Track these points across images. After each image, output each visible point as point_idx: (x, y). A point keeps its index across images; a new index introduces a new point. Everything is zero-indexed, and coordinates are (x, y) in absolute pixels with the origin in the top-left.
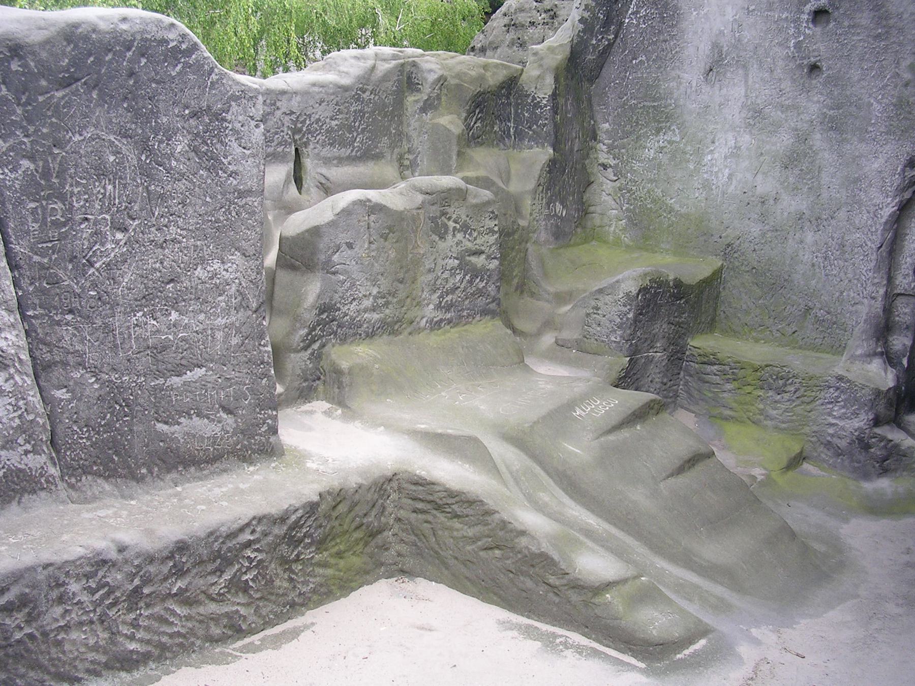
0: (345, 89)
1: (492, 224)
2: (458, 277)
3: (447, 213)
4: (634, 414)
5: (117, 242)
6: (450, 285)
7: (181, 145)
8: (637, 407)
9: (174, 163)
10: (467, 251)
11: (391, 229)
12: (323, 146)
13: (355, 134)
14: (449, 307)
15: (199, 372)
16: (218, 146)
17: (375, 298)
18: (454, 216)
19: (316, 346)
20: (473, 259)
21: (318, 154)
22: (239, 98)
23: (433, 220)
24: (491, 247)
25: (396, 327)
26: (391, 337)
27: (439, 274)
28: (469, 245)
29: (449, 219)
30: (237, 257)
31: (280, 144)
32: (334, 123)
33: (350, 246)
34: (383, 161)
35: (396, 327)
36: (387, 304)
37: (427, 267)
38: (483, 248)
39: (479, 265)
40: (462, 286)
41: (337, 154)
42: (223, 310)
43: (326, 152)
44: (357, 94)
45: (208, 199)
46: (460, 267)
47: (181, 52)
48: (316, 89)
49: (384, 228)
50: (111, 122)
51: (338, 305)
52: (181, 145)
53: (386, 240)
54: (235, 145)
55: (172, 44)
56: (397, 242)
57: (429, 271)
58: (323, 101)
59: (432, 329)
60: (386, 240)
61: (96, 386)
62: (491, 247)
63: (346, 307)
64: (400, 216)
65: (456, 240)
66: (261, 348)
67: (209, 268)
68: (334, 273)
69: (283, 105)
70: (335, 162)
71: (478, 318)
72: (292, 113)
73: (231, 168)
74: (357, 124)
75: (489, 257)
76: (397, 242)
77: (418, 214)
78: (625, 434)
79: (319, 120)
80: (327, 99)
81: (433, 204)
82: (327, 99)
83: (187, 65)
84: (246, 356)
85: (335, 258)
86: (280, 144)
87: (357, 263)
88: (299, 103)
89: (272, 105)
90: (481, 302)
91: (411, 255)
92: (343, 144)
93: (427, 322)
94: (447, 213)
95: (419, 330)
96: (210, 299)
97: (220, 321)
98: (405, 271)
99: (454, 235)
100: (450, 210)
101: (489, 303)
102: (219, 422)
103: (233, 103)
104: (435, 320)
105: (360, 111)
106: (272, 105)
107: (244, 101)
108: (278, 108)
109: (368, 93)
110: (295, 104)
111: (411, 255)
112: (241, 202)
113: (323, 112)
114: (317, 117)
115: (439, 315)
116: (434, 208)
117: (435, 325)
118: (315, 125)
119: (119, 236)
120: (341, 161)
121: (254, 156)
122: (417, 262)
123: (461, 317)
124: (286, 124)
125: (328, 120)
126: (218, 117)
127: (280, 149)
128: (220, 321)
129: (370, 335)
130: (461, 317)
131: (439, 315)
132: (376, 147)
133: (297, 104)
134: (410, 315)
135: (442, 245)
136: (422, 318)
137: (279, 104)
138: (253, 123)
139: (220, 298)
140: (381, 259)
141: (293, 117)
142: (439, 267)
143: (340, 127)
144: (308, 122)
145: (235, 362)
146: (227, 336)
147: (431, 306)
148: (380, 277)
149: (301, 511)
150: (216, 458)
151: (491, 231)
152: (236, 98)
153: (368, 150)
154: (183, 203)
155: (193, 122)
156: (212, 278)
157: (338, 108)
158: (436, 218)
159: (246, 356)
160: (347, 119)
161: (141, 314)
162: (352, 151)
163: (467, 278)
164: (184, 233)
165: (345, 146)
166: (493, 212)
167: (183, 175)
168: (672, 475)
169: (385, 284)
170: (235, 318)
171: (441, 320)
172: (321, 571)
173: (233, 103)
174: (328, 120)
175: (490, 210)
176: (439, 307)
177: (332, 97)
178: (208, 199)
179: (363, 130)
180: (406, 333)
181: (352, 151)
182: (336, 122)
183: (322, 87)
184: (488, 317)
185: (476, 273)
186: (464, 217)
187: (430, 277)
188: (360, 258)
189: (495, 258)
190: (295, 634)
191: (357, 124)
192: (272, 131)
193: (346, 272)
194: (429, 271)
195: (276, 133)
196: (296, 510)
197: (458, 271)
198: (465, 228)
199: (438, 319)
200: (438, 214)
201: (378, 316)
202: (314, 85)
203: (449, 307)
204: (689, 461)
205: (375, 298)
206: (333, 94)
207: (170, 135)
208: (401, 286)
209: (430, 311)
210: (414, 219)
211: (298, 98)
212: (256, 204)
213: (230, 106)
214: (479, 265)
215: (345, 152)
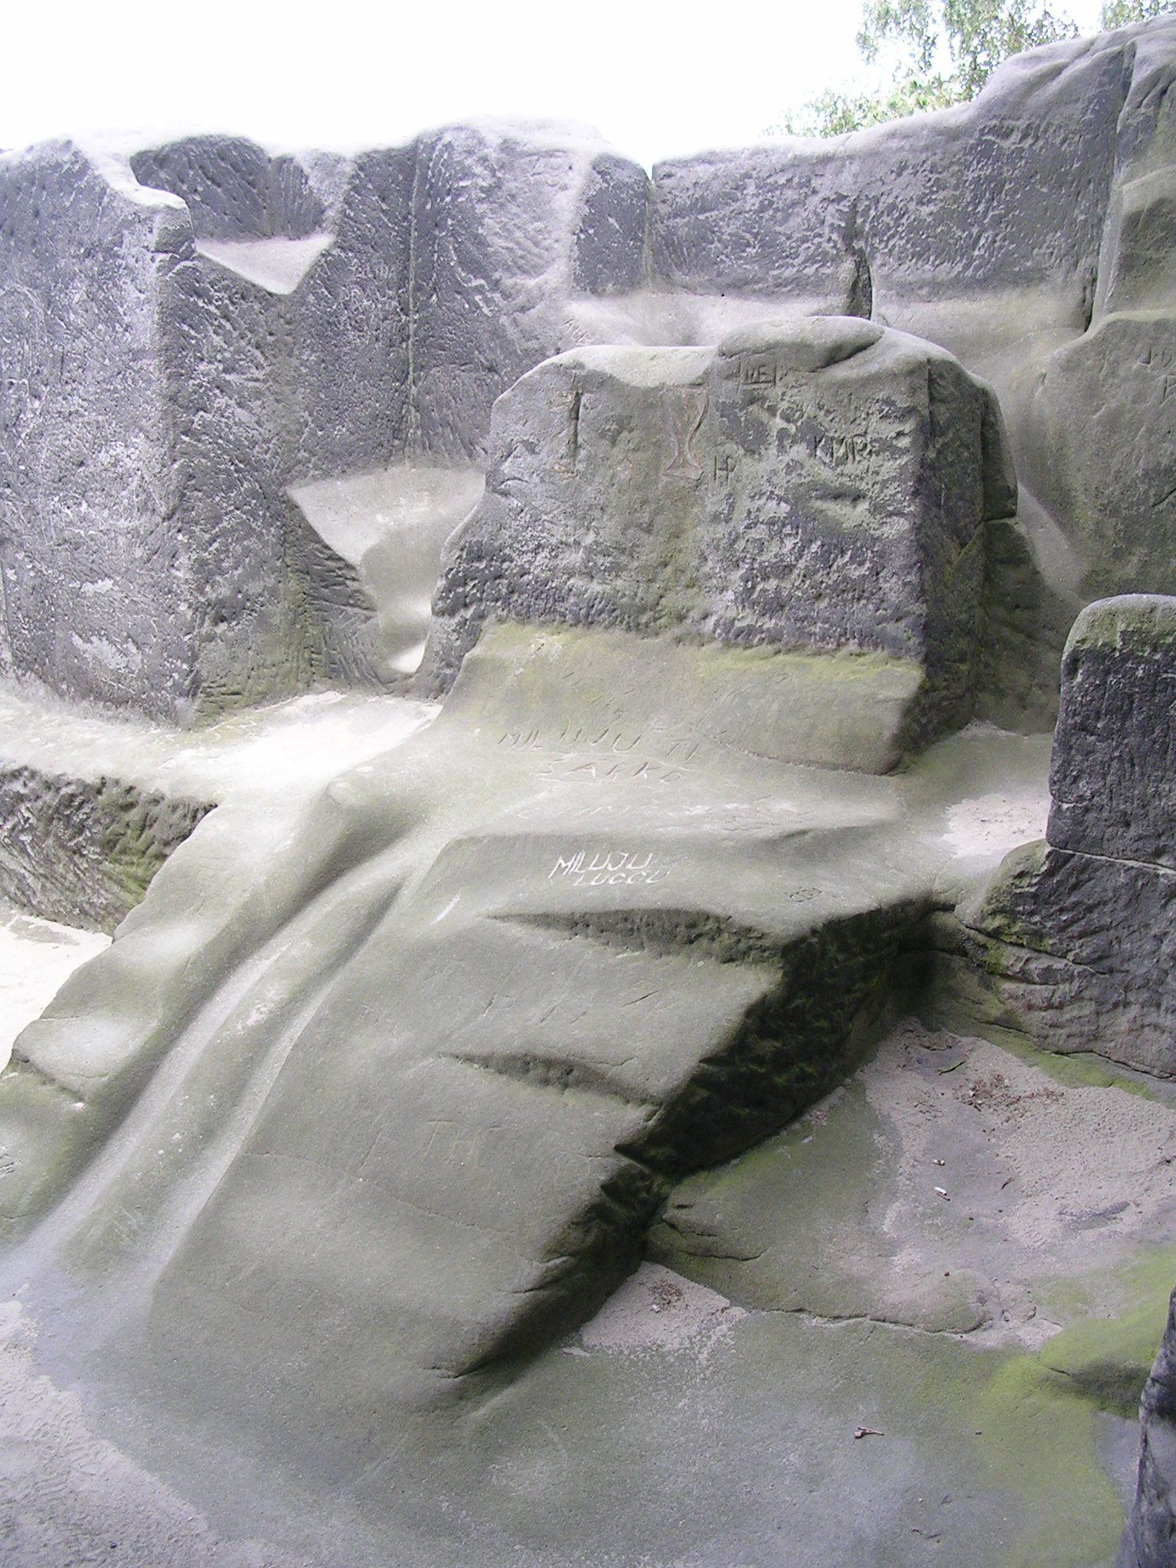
0: (952, 135)
1: (889, 430)
2: (789, 543)
3: (764, 399)
4: (626, 916)
5: (34, 411)
6: (768, 557)
7: (78, 294)
8: (643, 905)
9: (72, 317)
10: (814, 486)
11: (624, 424)
12: (901, 260)
13: (975, 231)
14: (775, 606)
15: (108, 584)
16: (114, 291)
17: (589, 550)
18: (784, 405)
19: (469, 613)
20: (835, 509)
21: (887, 277)
22: (132, 223)
23: (725, 410)
24: (884, 484)
25: (644, 619)
26: (632, 635)
27: (741, 529)
28: (826, 474)
29: (772, 411)
30: (140, 440)
31: (810, 260)
32: (925, 210)
33: (531, 448)
34: (1042, 287)
35: (644, 619)
36: (616, 569)
37: (710, 509)
38: (863, 486)
39: (847, 525)
40: (801, 564)
41: (928, 276)
42: (126, 509)
43: (906, 272)
44: (980, 142)
45: (107, 362)
46: (793, 520)
47: (74, 175)
48: (894, 144)
49: (607, 420)
50: (22, 272)
51: (507, 551)
52: (78, 294)
53: (613, 443)
54: (130, 287)
55: (66, 167)
56: (635, 450)
57: (715, 518)
58: (905, 168)
59: (728, 645)
60: (613, 443)
61: (32, 574)
62: (884, 484)
63: (526, 558)
64: (650, 400)
65: (786, 459)
66: (173, 571)
67: (112, 452)
68: (505, 494)
69: (825, 185)
70: (924, 292)
71: (853, 646)
72: (841, 198)
73: (127, 319)
74: (981, 208)
75: (876, 509)
76: (635, 450)
77: (691, 396)
78: (553, 942)
79: (893, 207)
80: (912, 162)
81: (728, 377)
82: (912, 162)
83: (80, 191)
84: (152, 577)
85: (506, 467)
86: (810, 260)
87: (542, 481)
88: (856, 176)
89: (801, 186)
90: (863, 612)
91: (665, 479)
92: (945, 254)
93: (716, 625)
94: (764, 399)
95: (701, 640)
96: (113, 492)
97: (123, 523)
98: (657, 512)
99: (781, 448)
100: (775, 392)
101: (884, 619)
102: (126, 655)
103: (126, 232)
104: (738, 624)
105: (989, 179)
106: (801, 186)
107: (138, 226)
108: (815, 192)
109: (1015, 137)
110: (847, 181)
111: (665, 479)
112: (136, 366)
113: (904, 189)
114: (890, 200)
115: (747, 618)
116: (730, 385)
117: (738, 637)
118: (885, 219)
119: (37, 404)
120: (936, 289)
121: (148, 301)
122: (687, 495)
123: (802, 634)
124: (829, 220)
125: (912, 206)
126: (110, 254)
127: (810, 271)
128: (123, 523)
129: (586, 619)
130: (802, 634)
131: (747, 618)
132: (1026, 257)
133: (850, 179)
134: (674, 600)
135: (748, 467)
136: (705, 617)
137: (816, 183)
138: (149, 255)
139: (124, 493)
140: (597, 479)
141: (844, 206)
142: (740, 515)
143: (940, 218)
144: (872, 213)
145: (140, 582)
146: (131, 545)
147: (730, 595)
148: (597, 513)
149: (73, 787)
150: (120, 702)
151: (887, 447)
152: (127, 224)
153: (1002, 265)
154: (82, 367)
155: (88, 262)
156: (114, 465)
157: (934, 177)
158: (734, 405)
159: (152, 577)
160: (956, 200)
161: (56, 499)
162: (966, 267)
163: (814, 547)
164: (85, 404)
165: (951, 260)
166: (888, 402)
167: (80, 331)
168: (486, 1062)
169: (609, 529)
170: (142, 522)
171: (750, 631)
172: (116, 888)
173: (126, 232)
174: (912, 206)
175: (881, 396)
176: (745, 598)
177: (924, 156)
178: (107, 362)
179: (998, 221)
180: (668, 635)
181: (966, 267)
182: (932, 208)
183: (906, 137)
184: (881, 654)
185: (837, 542)
186: (809, 410)
187: (721, 530)
188: (551, 473)
189: (899, 513)
190: (54, 938)
191: (981, 208)
192: (796, 236)
193: (521, 494)
194: (715, 518)
195: (805, 240)
196: (69, 784)
197: (788, 530)
198: (815, 438)
199: (744, 624)
200: (738, 398)
201: (599, 588)
202: (892, 135)
203: (775, 606)
204: (549, 1063)
205: (589, 550)
206: (926, 148)
207: (66, 280)
208: (648, 539)
209: (724, 604)
210: (683, 407)
211: (855, 168)
212: (151, 369)
213: (122, 236)
214: (847, 525)
215: (947, 271)
